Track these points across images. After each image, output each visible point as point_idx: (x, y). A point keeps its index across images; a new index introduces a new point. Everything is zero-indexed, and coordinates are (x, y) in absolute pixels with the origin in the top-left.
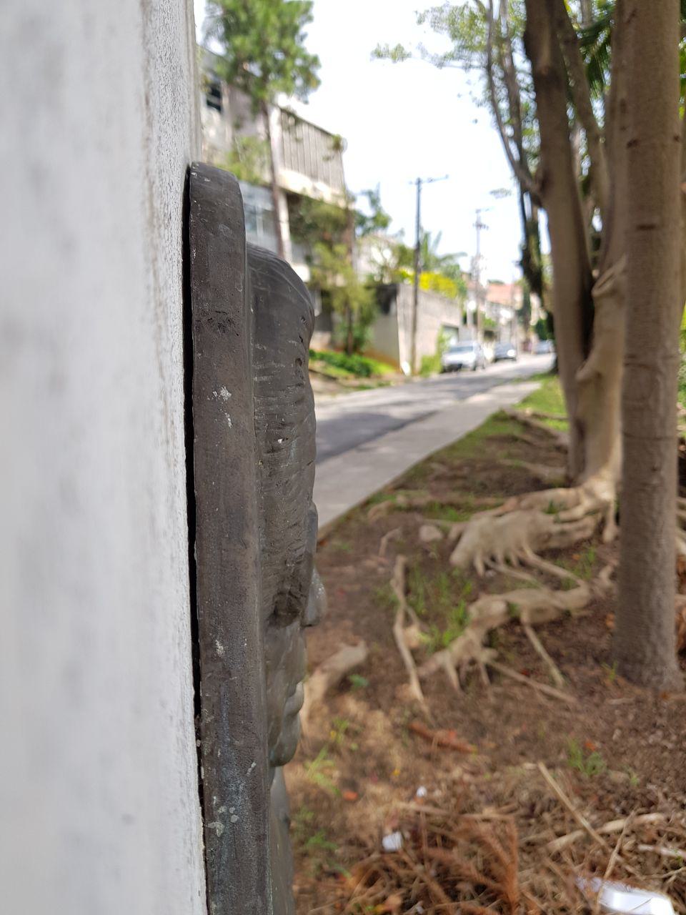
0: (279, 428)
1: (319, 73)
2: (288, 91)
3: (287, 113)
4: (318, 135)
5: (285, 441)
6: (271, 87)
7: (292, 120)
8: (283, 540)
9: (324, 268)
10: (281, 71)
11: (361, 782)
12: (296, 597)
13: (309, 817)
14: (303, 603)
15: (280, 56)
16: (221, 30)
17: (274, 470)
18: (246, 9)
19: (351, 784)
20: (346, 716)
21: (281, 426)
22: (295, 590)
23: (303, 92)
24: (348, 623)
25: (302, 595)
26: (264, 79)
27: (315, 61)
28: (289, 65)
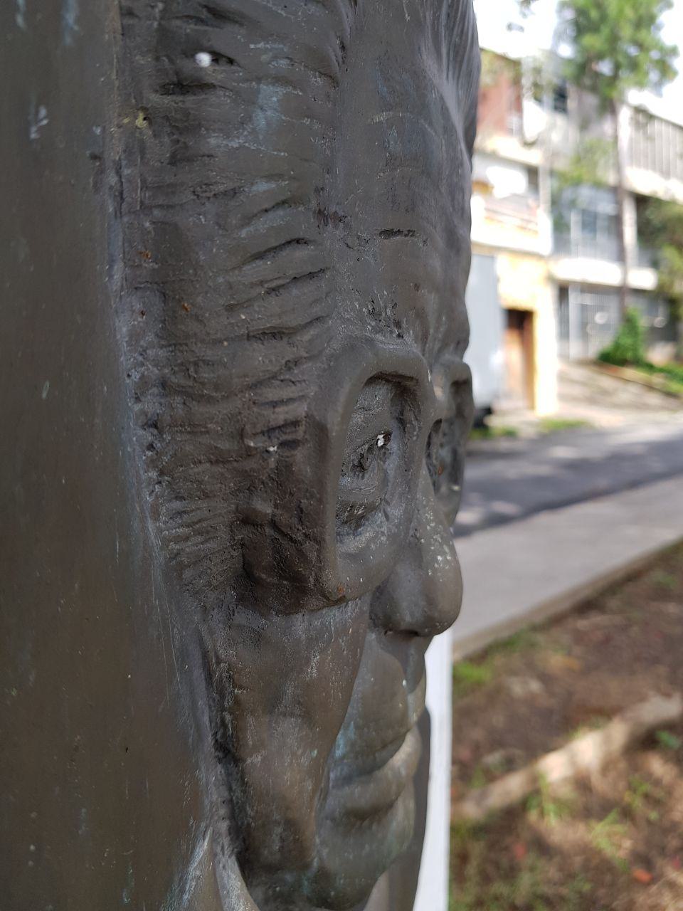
0: (200, 21)
1: (676, 63)
2: (641, 85)
3: (639, 110)
4: (671, 130)
5: (224, 67)
6: (621, 84)
7: (644, 116)
8: (225, 366)
9: (672, 273)
10: (634, 65)
11: (659, 862)
12: (291, 539)
13: (587, 887)
14: (313, 556)
15: (633, 51)
16: (571, 32)
17: (186, 147)
18: (599, 6)
19: (643, 859)
20: (649, 777)
21: (204, 14)
22: (284, 518)
23: (658, 86)
24: (662, 670)
25: (306, 535)
26: (615, 78)
27: (673, 51)
28: (642, 58)
